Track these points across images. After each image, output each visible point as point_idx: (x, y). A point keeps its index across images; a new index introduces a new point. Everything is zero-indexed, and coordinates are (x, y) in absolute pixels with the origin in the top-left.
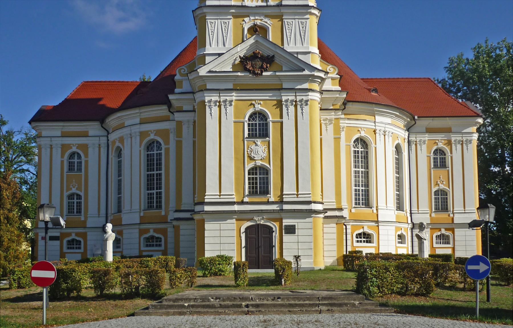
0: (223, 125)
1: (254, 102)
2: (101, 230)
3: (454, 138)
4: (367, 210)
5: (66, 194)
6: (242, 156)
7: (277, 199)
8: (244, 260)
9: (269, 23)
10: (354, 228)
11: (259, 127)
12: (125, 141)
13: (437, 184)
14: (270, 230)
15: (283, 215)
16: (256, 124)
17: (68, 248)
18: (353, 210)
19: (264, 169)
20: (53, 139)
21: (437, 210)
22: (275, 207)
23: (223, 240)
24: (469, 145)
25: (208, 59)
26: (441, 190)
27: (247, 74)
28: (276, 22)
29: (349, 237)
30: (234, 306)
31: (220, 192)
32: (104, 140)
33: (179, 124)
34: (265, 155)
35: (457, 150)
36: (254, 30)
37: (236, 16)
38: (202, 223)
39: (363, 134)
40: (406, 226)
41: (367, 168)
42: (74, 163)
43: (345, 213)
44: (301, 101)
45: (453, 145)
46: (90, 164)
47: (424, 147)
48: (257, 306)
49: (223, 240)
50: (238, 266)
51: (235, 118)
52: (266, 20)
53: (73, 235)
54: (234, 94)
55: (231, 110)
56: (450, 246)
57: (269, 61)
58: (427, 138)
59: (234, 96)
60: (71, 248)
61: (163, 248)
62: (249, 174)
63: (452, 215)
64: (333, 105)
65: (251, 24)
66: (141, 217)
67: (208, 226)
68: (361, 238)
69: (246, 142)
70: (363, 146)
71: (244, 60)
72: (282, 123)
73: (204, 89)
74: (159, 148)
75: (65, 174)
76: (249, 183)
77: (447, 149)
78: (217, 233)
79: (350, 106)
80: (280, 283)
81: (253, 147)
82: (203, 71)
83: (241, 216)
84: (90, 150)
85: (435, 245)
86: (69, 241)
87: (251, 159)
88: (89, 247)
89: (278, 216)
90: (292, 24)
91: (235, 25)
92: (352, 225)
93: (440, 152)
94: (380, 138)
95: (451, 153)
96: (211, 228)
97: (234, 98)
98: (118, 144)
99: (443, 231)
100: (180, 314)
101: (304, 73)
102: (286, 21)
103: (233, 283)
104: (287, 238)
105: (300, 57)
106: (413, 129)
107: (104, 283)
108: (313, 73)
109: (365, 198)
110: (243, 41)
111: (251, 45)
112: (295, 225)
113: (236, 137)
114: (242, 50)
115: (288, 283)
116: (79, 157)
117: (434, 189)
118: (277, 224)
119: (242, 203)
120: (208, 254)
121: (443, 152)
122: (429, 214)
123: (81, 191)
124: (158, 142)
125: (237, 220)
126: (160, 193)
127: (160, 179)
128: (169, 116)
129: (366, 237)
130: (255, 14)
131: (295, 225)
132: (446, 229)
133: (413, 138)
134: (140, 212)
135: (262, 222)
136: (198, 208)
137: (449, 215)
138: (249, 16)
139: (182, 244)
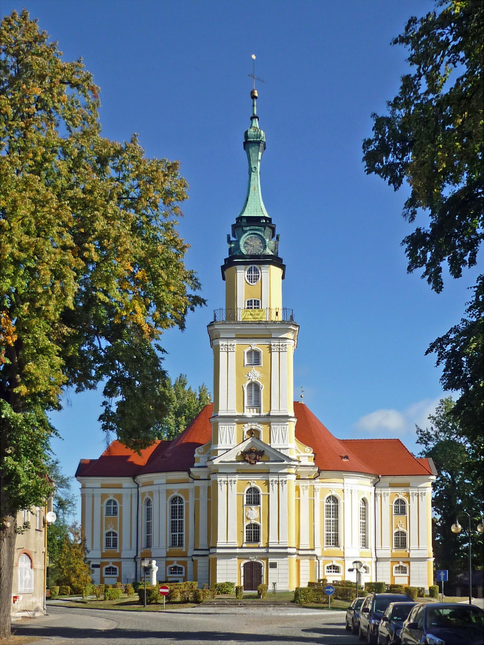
0: (230, 495)
1: (250, 481)
2: (133, 560)
3: (411, 491)
4: (337, 549)
5: (105, 532)
6: (241, 517)
7: (265, 545)
8: (242, 584)
9: (261, 428)
10: (325, 562)
11: (253, 498)
12: (154, 495)
13: (397, 527)
14: (260, 566)
15: (268, 556)
16: (251, 495)
17: (106, 574)
18: (325, 549)
19: (256, 525)
20: (94, 489)
21: (397, 546)
22: (264, 550)
23: (229, 572)
24: (423, 497)
25: (220, 453)
26: (401, 532)
27: (246, 463)
28: (266, 427)
29: (321, 568)
30: (235, 604)
31: (227, 540)
32: (135, 491)
33: (197, 489)
34: (258, 516)
35: (414, 501)
36: (251, 432)
37: (238, 423)
38: (215, 560)
39: (334, 493)
40: (370, 559)
41: (338, 518)
42: (112, 509)
43: (318, 552)
44: (282, 481)
45: (411, 497)
46: (124, 509)
47: (388, 498)
48: (245, 604)
49: (229, 572)
50: (237, 588)
51: (238, 492)
52: (259, 426)
53: (111, 563)
54: (237, 476)
55: (235, 486)
56: (407, 575)
57: (261, 453)
58: (390, 492)
59: (237, 477)
60: (108, 574)
61: (183, 575)
62: (247, 528)
63: (408, 551)
64: (309, 476)
65: (249, 428)
66: (167, 553)
67: (219, 562)
68: (331, 569)
69: (245, 508)
70: (334, 501)
71: (244, 454)
72: (269, 495)
73: (216, 473)
74: (181, 501)
75: (104, 517)
76: (247, 535)
77: (406, 500)
78: (225, 567)
79: (323, 474)
80: (260, 597)
81: (249, 511)
82: (216, 462)
83: (241, 556)
84: (124, 498)
85: (394, 574)
86: (106, 568)
87: (248, 519)
88: (123, 573)
89: (266, 556)
90: (277, 428)
91: (238, 428)
92: (324, 560)
93: (400, 502)
94: (347, 495)
95: (409, 503)
96: (221, 565)
97: (237, 479)
98: (147, 496)
99: (401, 564)
100: (214, 607)
101: (284, 463)
102: (272, 426)
103: (235, 597)
104: (271, 570)
105: (282, 451)
106: (378, 485)
107: (171, 596)
108: (290, 463)
109: (334, 540)
110: (244, 441)
111: (248, 444)
112: (276, 563)
113: (238, 504)
114: (243, 447)
115: (264, 597)
116: (115, 503)
117: (395, 531)
118: (265, 562)
119: (242, 547)
120: (219, 581)
121: (403, 501)
122: (390, 551)
123: (116, 529)
124: (179, 497)
125: (238, 558)
126: (182, 535)
127: (182, 525)
128: (188, 480)
129: (336, 569)
130: (251, 422)
131: (276, 563)
132: (404, 562)
133: (378, 491)
134: (166, 548)
135: (255, 560)
136: (212, 551)
137: (406, 551)
138: (247, 423)
139: (199, 573)
